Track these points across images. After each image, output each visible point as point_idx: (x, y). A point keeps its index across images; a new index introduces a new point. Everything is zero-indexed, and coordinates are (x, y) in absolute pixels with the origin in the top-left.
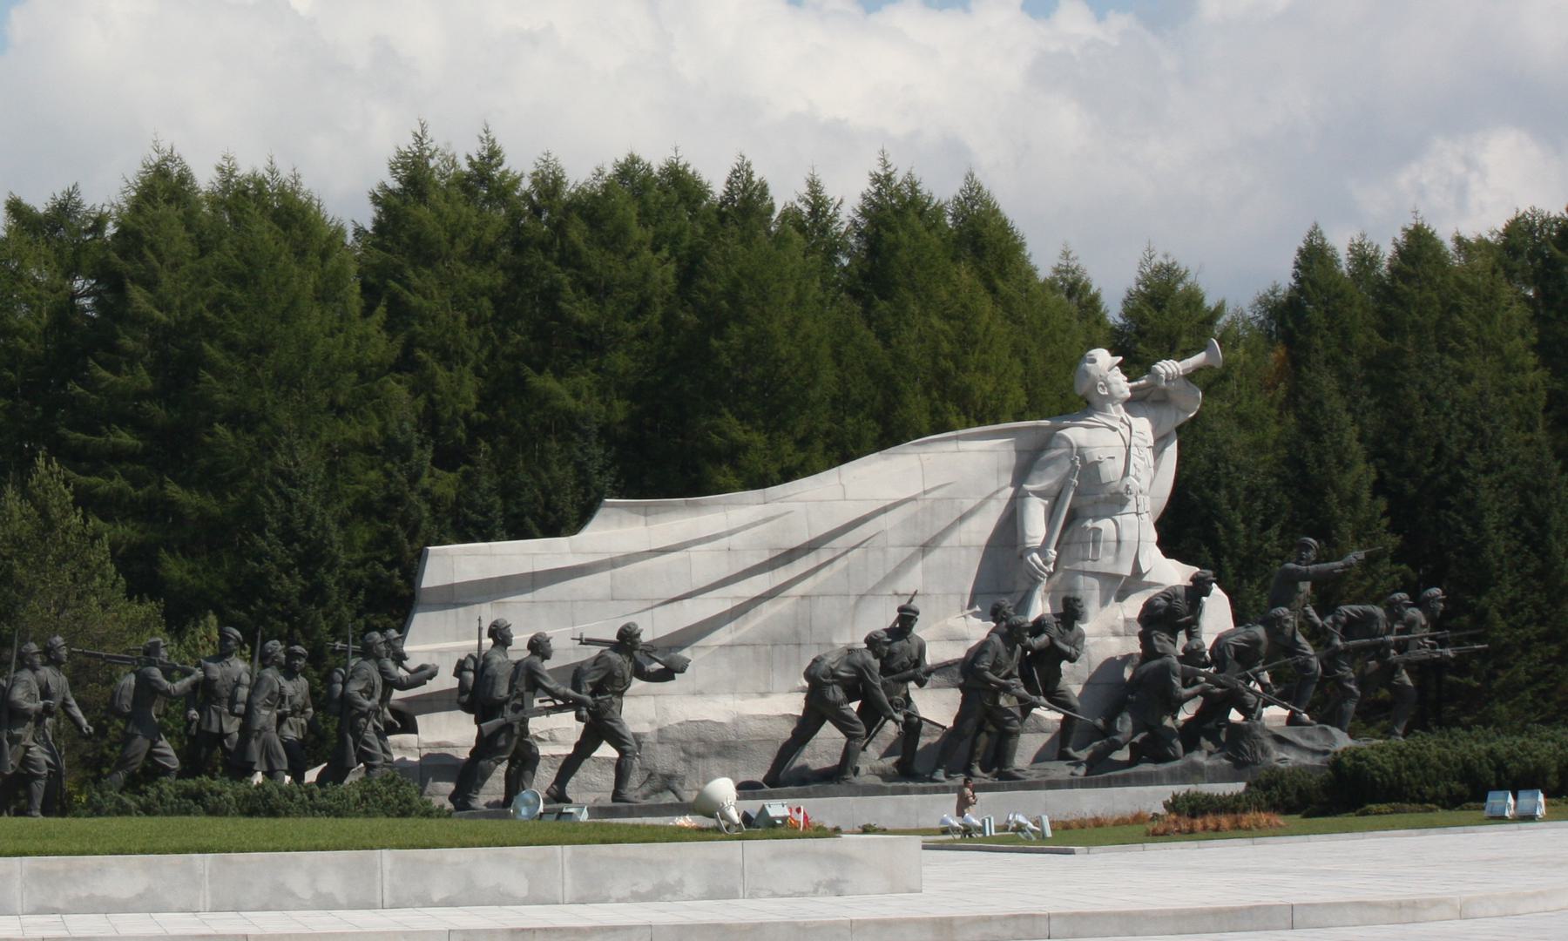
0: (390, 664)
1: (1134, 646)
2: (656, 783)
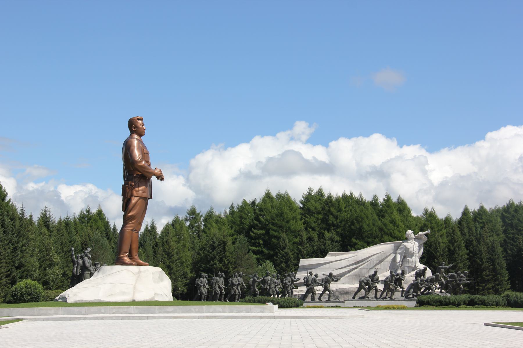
0: (293, 278)
1: (414, 279)
2: (336, 297)
